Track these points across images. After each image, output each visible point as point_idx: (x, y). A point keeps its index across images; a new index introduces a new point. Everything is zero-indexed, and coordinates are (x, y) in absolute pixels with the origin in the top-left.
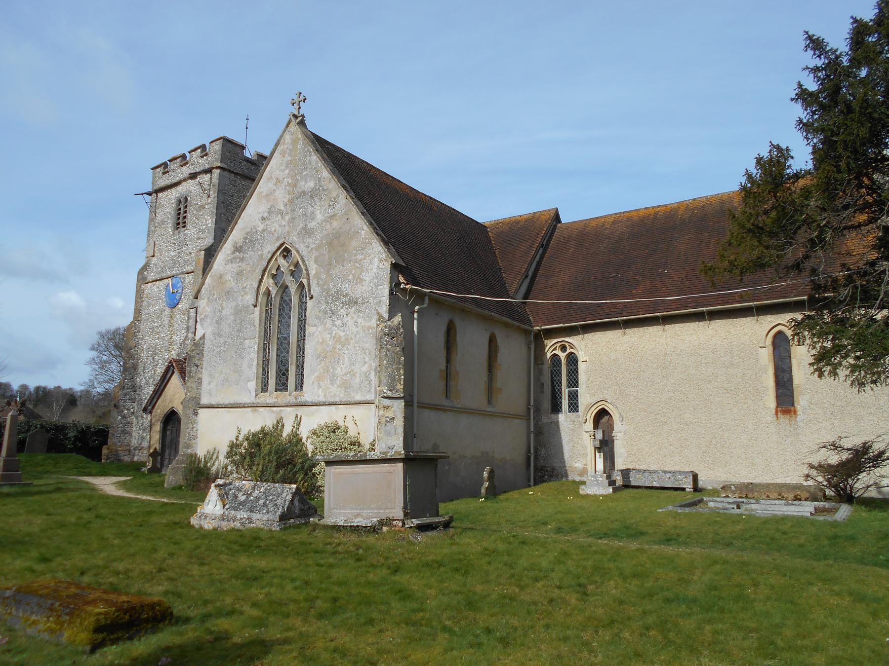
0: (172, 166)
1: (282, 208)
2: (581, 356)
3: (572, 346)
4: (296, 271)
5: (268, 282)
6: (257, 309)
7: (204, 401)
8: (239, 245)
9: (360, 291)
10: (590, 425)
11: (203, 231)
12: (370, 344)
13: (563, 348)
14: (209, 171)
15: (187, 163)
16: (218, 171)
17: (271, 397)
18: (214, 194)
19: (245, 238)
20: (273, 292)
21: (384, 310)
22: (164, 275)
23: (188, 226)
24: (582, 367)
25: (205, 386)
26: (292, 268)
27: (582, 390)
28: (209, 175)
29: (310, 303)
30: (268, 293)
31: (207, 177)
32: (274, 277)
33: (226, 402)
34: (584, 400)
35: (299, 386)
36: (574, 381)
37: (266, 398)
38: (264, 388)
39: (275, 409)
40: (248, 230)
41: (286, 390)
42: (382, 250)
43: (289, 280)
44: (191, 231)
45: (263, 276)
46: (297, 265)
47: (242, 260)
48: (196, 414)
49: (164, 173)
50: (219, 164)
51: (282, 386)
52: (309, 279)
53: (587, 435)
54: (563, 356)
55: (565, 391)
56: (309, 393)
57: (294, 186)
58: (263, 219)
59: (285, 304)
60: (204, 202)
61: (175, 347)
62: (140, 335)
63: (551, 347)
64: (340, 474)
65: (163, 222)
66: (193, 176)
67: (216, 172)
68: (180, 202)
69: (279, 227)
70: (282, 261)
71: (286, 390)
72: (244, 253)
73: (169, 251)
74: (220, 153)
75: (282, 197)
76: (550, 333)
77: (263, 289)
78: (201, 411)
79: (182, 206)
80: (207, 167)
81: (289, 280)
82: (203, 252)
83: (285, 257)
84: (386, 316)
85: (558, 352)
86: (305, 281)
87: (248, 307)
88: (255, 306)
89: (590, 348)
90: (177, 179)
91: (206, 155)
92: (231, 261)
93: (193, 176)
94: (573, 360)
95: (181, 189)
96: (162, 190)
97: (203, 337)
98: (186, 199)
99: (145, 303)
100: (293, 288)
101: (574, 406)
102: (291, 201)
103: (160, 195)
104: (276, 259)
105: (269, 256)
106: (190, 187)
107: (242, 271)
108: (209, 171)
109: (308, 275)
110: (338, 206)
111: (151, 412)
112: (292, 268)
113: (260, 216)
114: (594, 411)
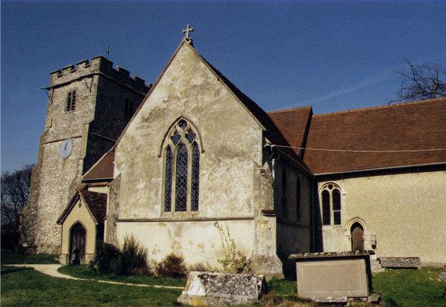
0: (65, 72)
1: (179, 95)
2: (342, 192)
3: (336, 185)
4: (190, 136)
5: (169, 141)
6: (161, 159)
7: (121, 217)
8: (146, 118)
9: (240, 147)
10: (348, 232)
11: (87, 113)
12: (249, 181)
13: (330, 187)
14: (91, 76)
15: (75, 71)
16: (97, 76)
17: (173, 214)
18: (94, 90)
19: (150, 114)
20: (173, 147)
21: (259, 159)
22: (58, 138)
23: (76, 109)
24: (343, 198)
25: (122, 208)
26: (186, 132)
27: (343, 212)
28: (91, 79)
29: (202, 156)
30: (169, 148)
31: (89, 80)
32: (172, 138)
33: (245, 216)
34: (345, 216)
35: (195, 207)
36: (337, 205)
37: (168, 215)
38: (168, 208)
39: (176, 223)
40: (153, 108)
41: (186, 210)
42: (257, 126)
43: (184, 140)
44: (78, 112)
45: (165, 137)
46: (190, 130)
47: (148, 127)
48: (115, 225)
49: (59, 77)
50: (98, 72)
51: (181, 206)
52: (201, 139)
53: (347, 238)
54: (330, 191)
55: (332, 212)
56: (205, 210)
57: (188, 82)
58: (164, 102)
59: (182, 158)
60: (87, 95)
61: (67, 183)
62: (41, 175)
63: (321, 187)
64: (309, 267)
65: (58, 106)
66: (80, 79)
67: (96, 77)
68: (70, 94)
69: (177, 109)
70: (179, 128)
71: (186, 210)
72: (150, 122)
73: (62, 124)
74: (99, 65)
75: (179, 88)
76: (323, 178)
77: (165, 146)
78: (118, 223)
79: (72, 96)
80: (90, 73)
81: (184, 140)
82: (88, 125)
83: (180, 126)
84: (260, 164)
85: (327, 189)
86: (198, 142)
87: (154, 157)
88: (159, 157)
89: (347, 188)
90: (69, 80)
91: (89, 66)
92: (142, 127)
93: (80, 79)
94: (337, 194)
95: (71, 86)
96: (58, 86)
97: (120, 175)
98: (74, 92)
99: (45, 156)
100: (189, 147)
101: (338, 221)
102: (186, 91)
103: (56, 90)
104: (175, 127)
105: (170, 124)
106: (79, 86)
107: (149, 134)
108: (91, 76)
109: (200, 137)
110: (221, 95)
111: (62, 224)
112: (186, 132)
113: (162, 100)
114: (351, 224)
